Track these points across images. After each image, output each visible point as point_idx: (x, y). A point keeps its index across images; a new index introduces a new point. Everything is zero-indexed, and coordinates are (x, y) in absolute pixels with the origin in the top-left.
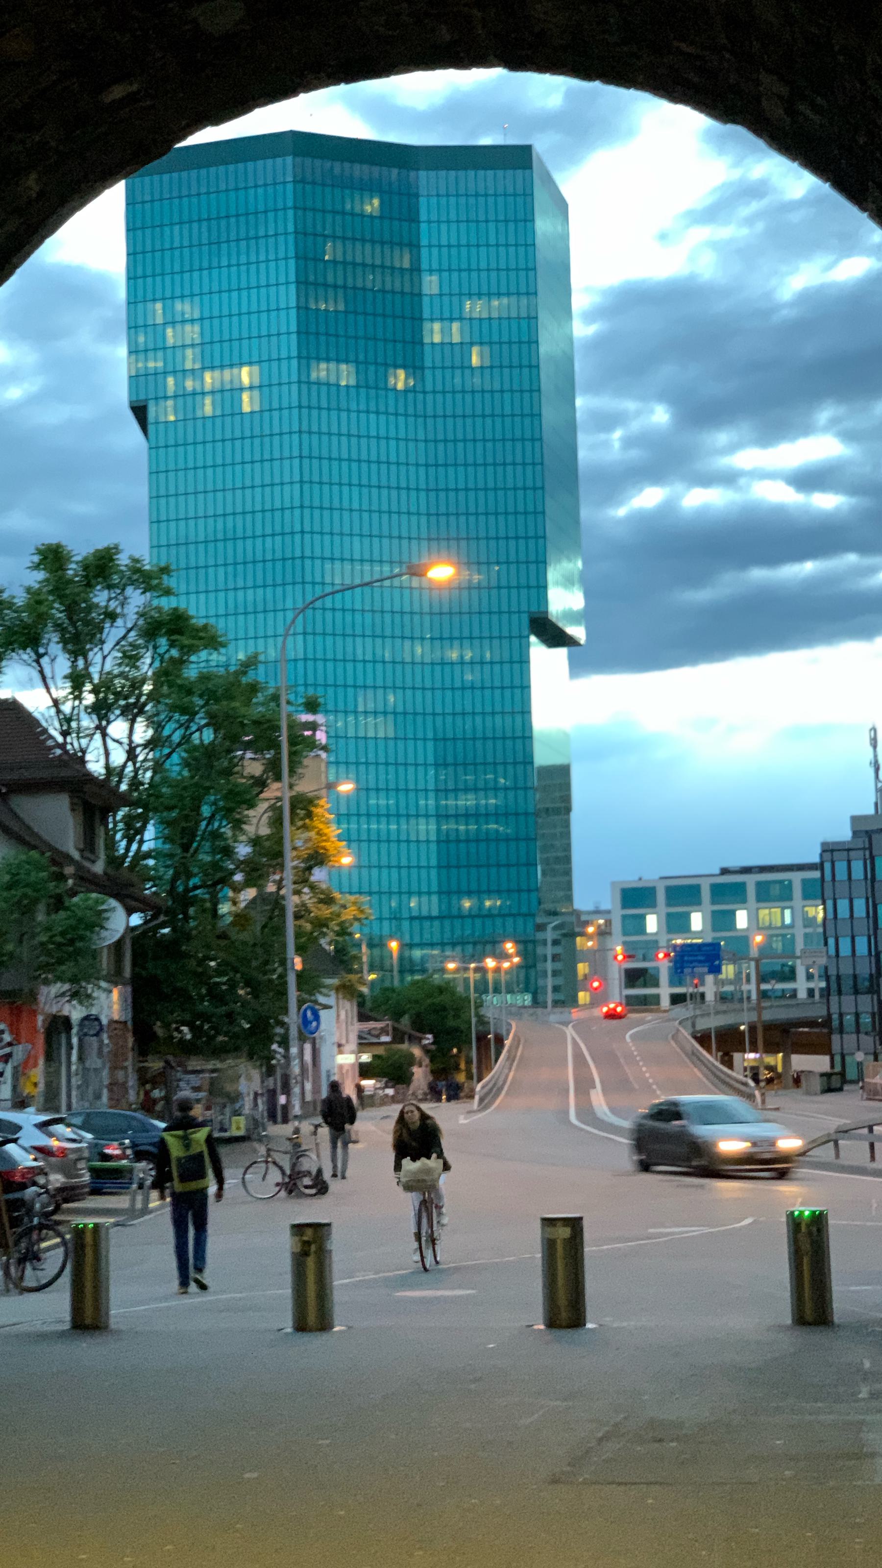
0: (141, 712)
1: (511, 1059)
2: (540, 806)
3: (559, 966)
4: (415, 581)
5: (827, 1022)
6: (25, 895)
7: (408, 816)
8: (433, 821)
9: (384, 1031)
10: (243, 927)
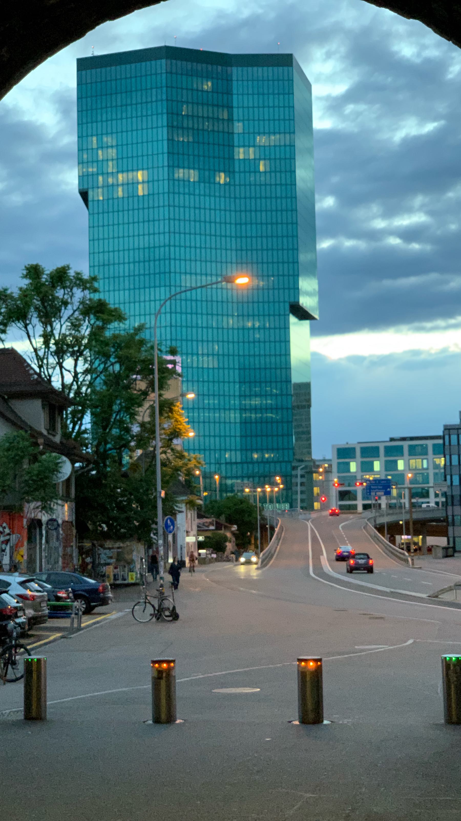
0: (81, 354)
1: (278, 539)
2: (295, 404)
3: (304, 488)
4: (229, 286)
5: (446, 520)
6: (17, 455)
7: (225, 409)
8: (238, 412)
9: (211, 524)
10: (135, 471)
